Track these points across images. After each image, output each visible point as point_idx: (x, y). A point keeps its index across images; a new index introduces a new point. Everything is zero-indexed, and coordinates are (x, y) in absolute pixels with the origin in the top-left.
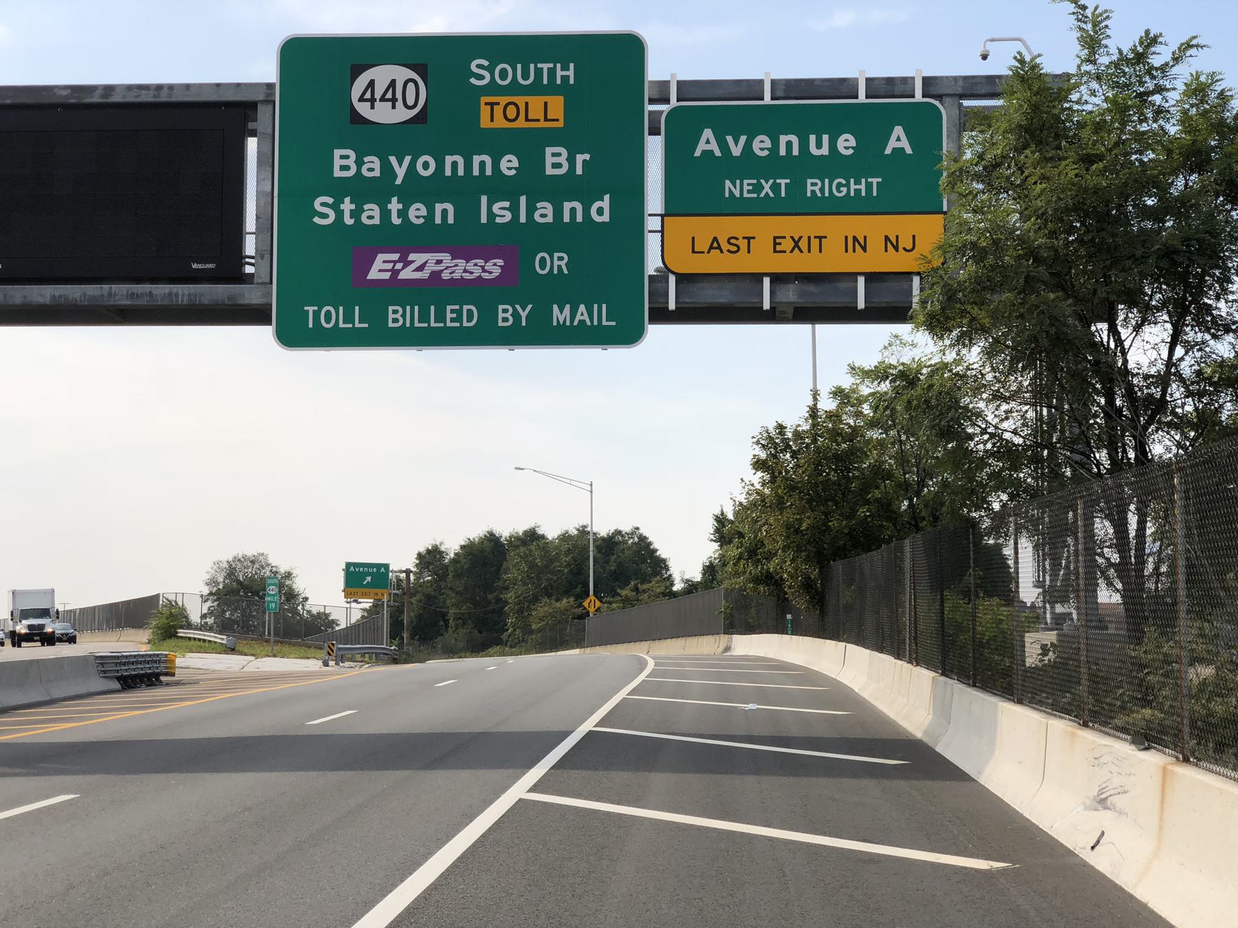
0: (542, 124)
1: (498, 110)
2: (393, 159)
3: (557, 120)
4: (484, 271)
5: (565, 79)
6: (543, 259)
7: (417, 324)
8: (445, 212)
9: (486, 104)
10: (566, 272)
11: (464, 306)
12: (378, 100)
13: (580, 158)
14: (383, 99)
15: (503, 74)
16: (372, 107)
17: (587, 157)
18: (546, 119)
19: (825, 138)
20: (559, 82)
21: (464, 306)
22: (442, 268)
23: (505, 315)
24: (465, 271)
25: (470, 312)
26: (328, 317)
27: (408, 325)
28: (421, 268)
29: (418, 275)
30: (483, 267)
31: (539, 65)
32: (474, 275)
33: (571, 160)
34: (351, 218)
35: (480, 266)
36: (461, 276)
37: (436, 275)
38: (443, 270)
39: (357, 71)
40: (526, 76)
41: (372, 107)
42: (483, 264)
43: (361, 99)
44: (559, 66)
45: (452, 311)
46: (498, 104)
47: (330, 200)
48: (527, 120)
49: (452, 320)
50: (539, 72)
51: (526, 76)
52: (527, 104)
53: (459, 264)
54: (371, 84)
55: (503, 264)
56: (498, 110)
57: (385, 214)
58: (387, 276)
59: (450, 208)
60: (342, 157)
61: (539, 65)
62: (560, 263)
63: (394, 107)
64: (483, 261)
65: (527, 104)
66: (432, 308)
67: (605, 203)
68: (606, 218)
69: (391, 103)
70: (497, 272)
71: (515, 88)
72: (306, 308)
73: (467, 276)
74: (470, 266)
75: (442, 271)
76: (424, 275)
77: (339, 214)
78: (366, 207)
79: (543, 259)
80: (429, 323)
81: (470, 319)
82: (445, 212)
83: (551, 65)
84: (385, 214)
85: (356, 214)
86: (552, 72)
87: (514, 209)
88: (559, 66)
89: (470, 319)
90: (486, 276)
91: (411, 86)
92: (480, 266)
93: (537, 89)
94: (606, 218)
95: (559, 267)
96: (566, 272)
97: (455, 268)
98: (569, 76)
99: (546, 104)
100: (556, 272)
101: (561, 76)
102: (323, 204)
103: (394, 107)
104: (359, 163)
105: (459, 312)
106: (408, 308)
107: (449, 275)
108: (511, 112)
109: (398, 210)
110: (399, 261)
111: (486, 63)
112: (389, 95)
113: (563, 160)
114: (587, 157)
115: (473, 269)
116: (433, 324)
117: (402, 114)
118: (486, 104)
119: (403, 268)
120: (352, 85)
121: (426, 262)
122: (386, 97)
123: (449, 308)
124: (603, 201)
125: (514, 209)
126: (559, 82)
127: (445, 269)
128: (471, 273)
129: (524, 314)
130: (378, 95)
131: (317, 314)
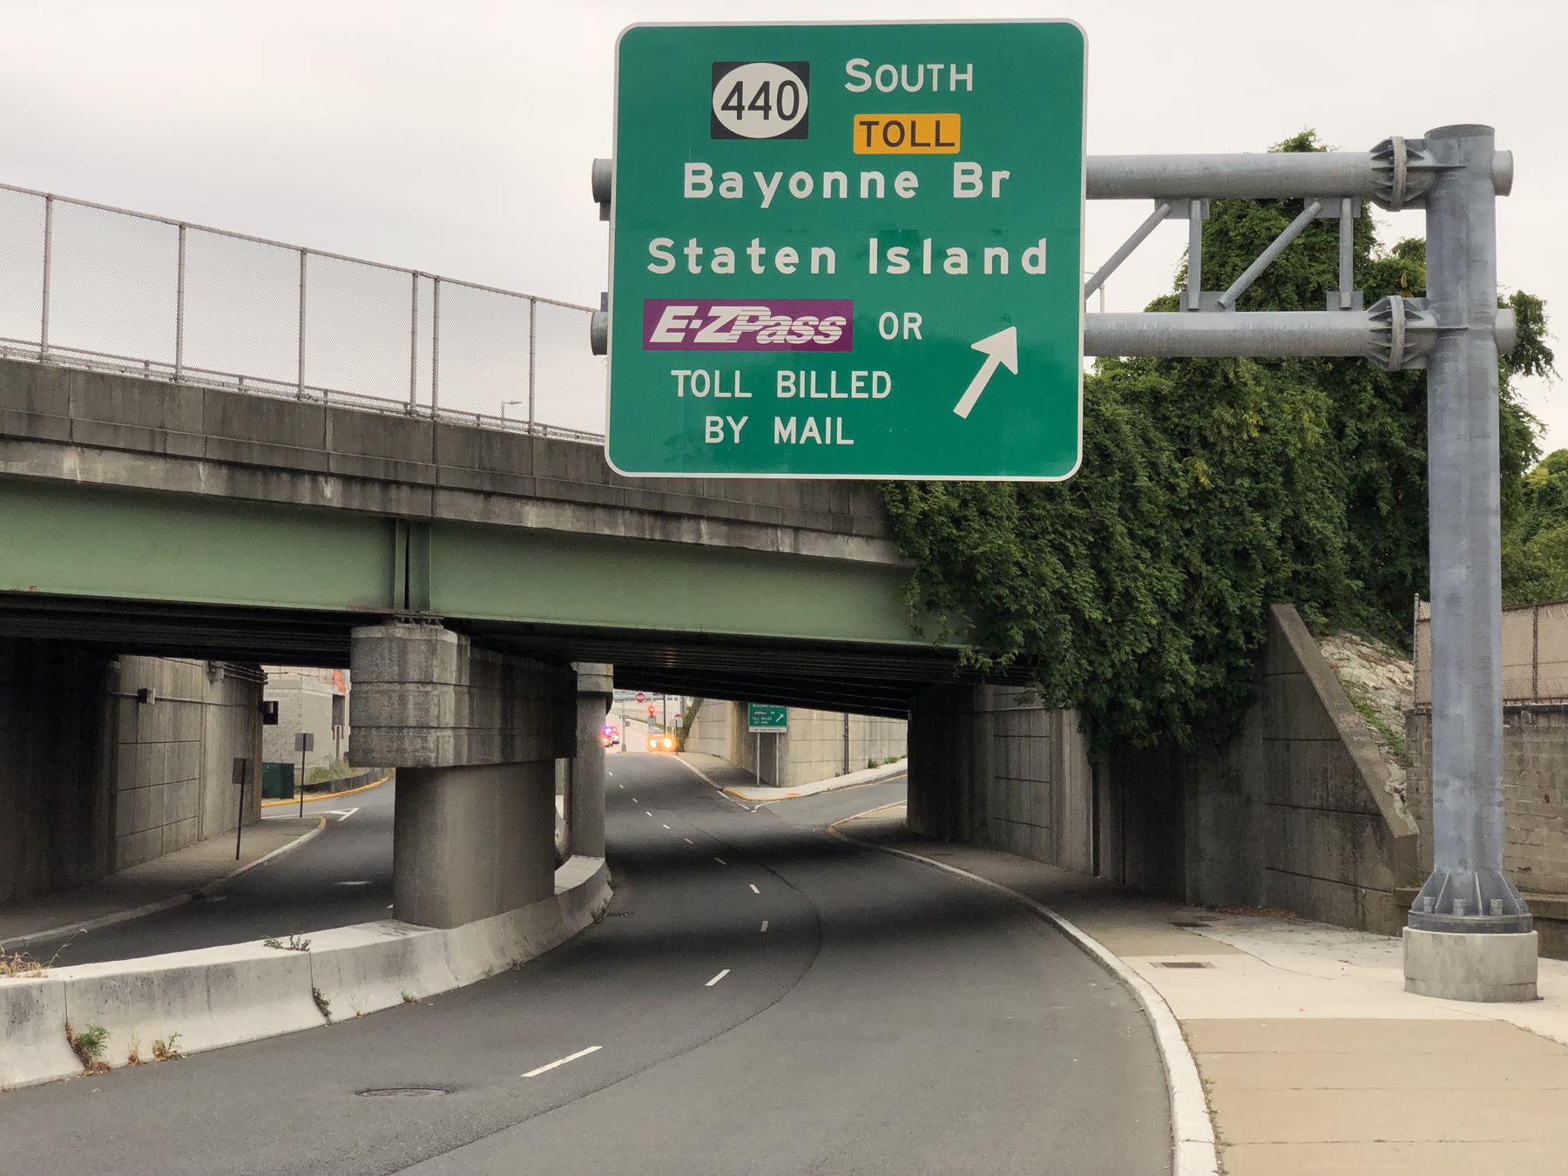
0: (934, 150)
1: (877, 132)
2: (759, 176)
3: (953, 145)
4: (818, 333)
5: (961, 84)
6: (889, 320)
7: (814, 395)
8: (823, 259)
9: (862, 123)
10: (919, 337)
11: (874, 372)
12: (746, 108)
13: (998, 176)
14: (752, 107)
15: (887, 78)
16: (739, 117)
17: (1006, 174)
18: (938, 143)
19: (827, 194)
20: (953, 88)
21: (874, 372)
22: (758, 328)
23: (786, 384)
24: (791, 332)
25: (881, 380)
26: (701, 384)
27: (802, 395)
28: (727, 328)
29: (723, 338)
30: (816, 327)
31: (929, 66)
32: (803, 338)
33: (986, 180)
34: (760, 265)
35: (811, 326)
36: (785, 340)
37: (748, 339)
38: (760, 330)
39: (720, 70)
40: (912, 80)
41: (739, 117)
42: (817, 323)
43: (725, 107)
44: (953, 67)
45: (859, 379)
46: (877, 123)
47: (669, 243)
48: (914, 144)
49: (859, 390)
50: (928, 73)
51: (912, 80)
52: (913, 123)
53: (782, 323)
54: (738, 87)
55: (845, 323)
56: (877, 132)
57: (743, 260)
58: (678, 338)
59: (830, 253)
60: (964, 172)
61: (929, 66)
62: (912, 325)
63: (766, 117)
64: (790, 319)
65: (913, 123)
66: (834, 373)
67: (1041, 250)
68: (1041, 269)
69: (763, 112)
70: (836, 334)
71: (900, 101)
72: (674, 373)
73: (793, 340)
74: (798, 325)
75: (756, 332)
76: (732, 337)
77: (682, 260)
78: (717, 251)
79: (889, 320)
80: (733, 393)
81: (881, 388)
82: (823, 259)
83: (942, 66)
84: (743, 260)
85: (704, 260)
86: (944, 74)
87: (916, 261)
88: (953, 67)
89: (881, 388)
90: (820, 340)
91: (788, 90)
92: (811, 326)
93: (927, 101)
94: (1041, 269)
95: (911, 330)
96: (919, 337)
97: (776, 328)
98: (965, 81)
99: (938, 123)
100: (906, 337)
101: (957, 81)
102: (661, 248)
103: (766, 117)
104: (717, 180)
105: (868, 380)
106: (802, 373)
107: (767, 338)
108: (894, 135)
109: (760, 255)
110: (697, 317)
111: (865, 63)
112: (761, 102)
113: (976, 179)
114: (1006, 174)
115: (804, 329)
116: (834, 395)
117: (777, 126)
118: (862, 123)
119: (703, 326)
120: (713, 89)
121: (735, 319)
122: (730, 105)
123: (855, 374)
124: (1038, 247)
125: (916, 261)
126: (953, 88)
127: (763, 329)
128: (800, 335)
129: (737, 429)
130: (746, 102)
131: (687, 379)
